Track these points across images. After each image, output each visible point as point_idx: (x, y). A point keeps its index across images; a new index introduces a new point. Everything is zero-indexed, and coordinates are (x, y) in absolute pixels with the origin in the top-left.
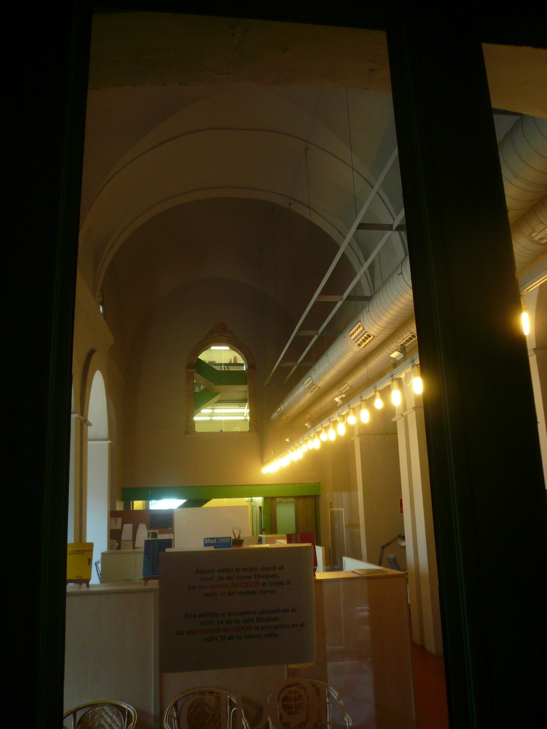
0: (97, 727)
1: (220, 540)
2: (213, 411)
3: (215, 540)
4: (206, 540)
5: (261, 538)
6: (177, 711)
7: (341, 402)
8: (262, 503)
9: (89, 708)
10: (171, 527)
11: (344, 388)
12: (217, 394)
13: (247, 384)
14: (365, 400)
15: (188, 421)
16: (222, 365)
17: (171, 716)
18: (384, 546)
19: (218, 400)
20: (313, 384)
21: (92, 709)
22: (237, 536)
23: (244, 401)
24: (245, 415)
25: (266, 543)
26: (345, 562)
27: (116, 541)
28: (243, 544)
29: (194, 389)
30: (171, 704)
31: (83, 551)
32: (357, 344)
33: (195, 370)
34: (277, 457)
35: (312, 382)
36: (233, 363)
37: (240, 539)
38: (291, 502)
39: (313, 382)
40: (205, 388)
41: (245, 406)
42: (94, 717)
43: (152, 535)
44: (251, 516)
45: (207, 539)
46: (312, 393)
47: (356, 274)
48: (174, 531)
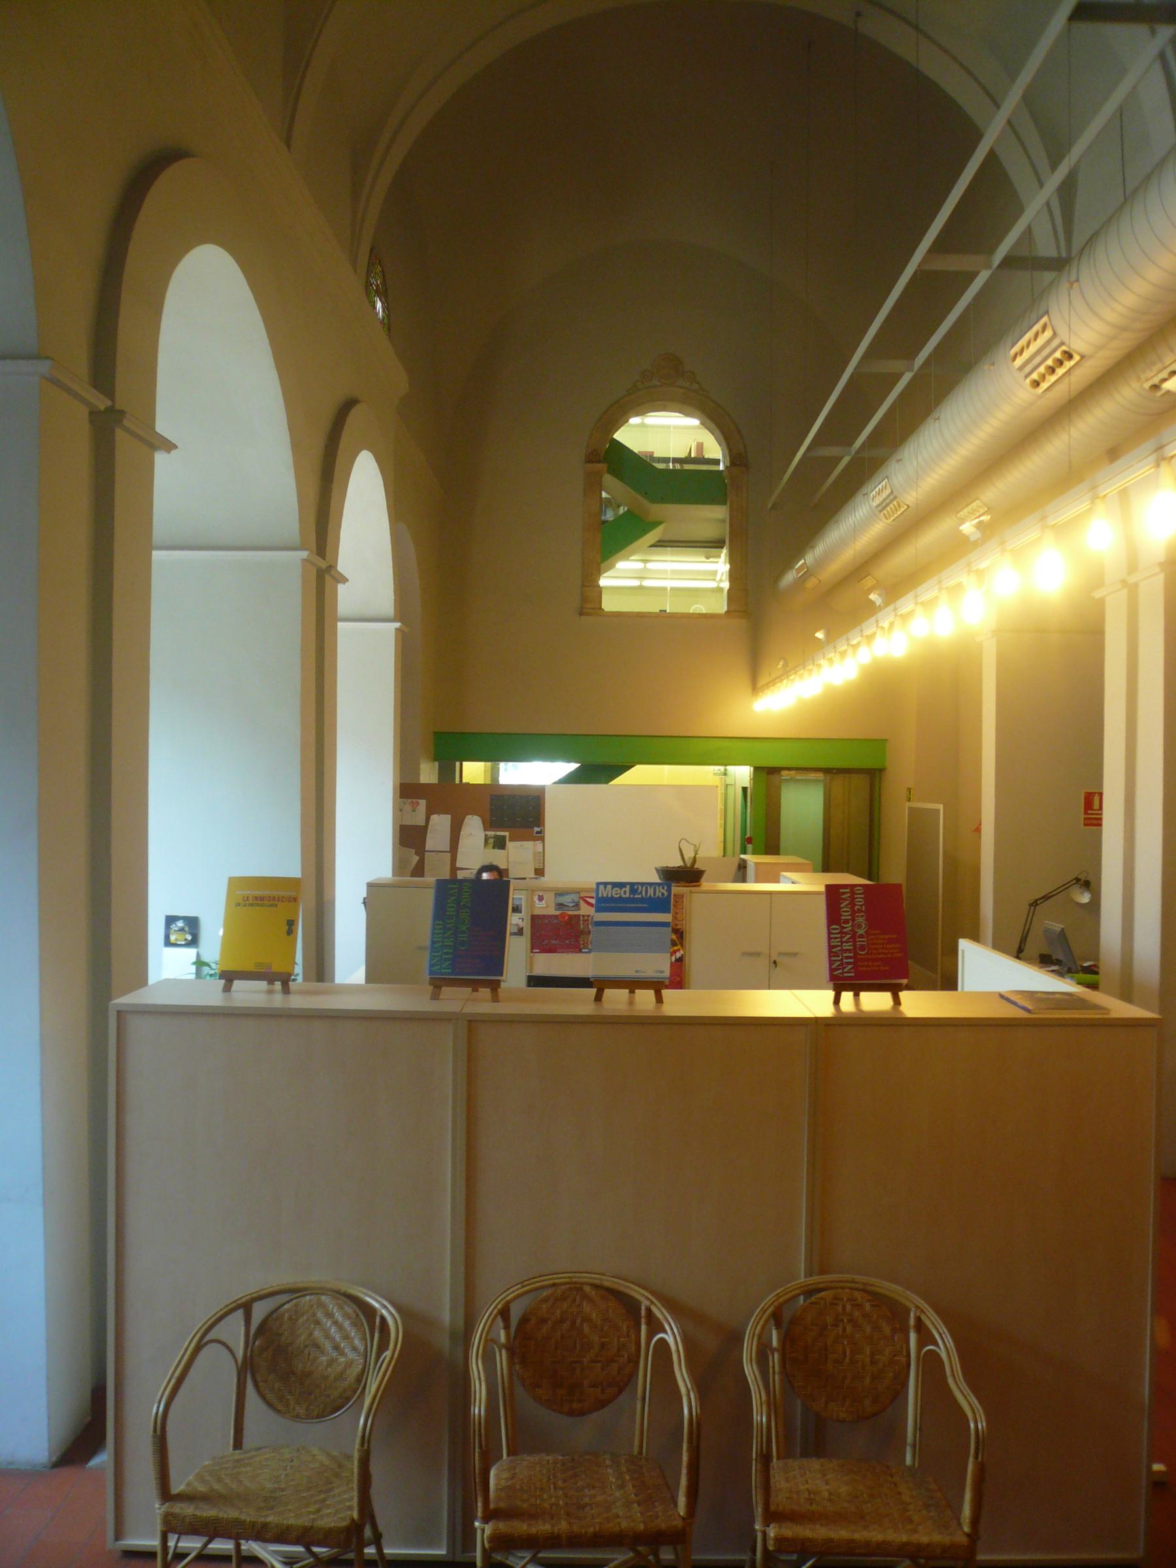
0: (302, 1346)
1: (639, 891)
2: (645, 566)
3: (628, 889)
4: (602, 887)
5: (744, 861)
6: (507, 1327)
7: (978, 535)
8: (749, 779)
9: (284, 1298)
10: (539, 827)
11: (970, 511)
12: (656, 524)
13: (725, 504)
14: (1054, 525)
15: (586, 586)
16: (670, 462)
17: (490, 1341)
18: (1037, 900)
19: (657, 540)
20: (892, 497)
21: (291, 1300)
22: (689, 865)
23: (718, 544)
24: (718, 578)
25: (757, 881)
26: (963, 951)
27: (413, 851)
28: (702, 880)
29: (601, 512)
30: (494, 1309)
31: (274, 899)
32: (1028, 381)
33: (603, 466)
34: (791, 676)
35: (890, 491)
36: (695, 458)
37: (696, 866)
38: (817, 781)
39: (892, 492)
40: (628, 510)
41: (720, 557)
42: (297, 1319)
43: (494, 842)
44: (723, 807)
45: (606, 884)
46: (889, 521)
47: (1021, 210)
48: (544, 836)
